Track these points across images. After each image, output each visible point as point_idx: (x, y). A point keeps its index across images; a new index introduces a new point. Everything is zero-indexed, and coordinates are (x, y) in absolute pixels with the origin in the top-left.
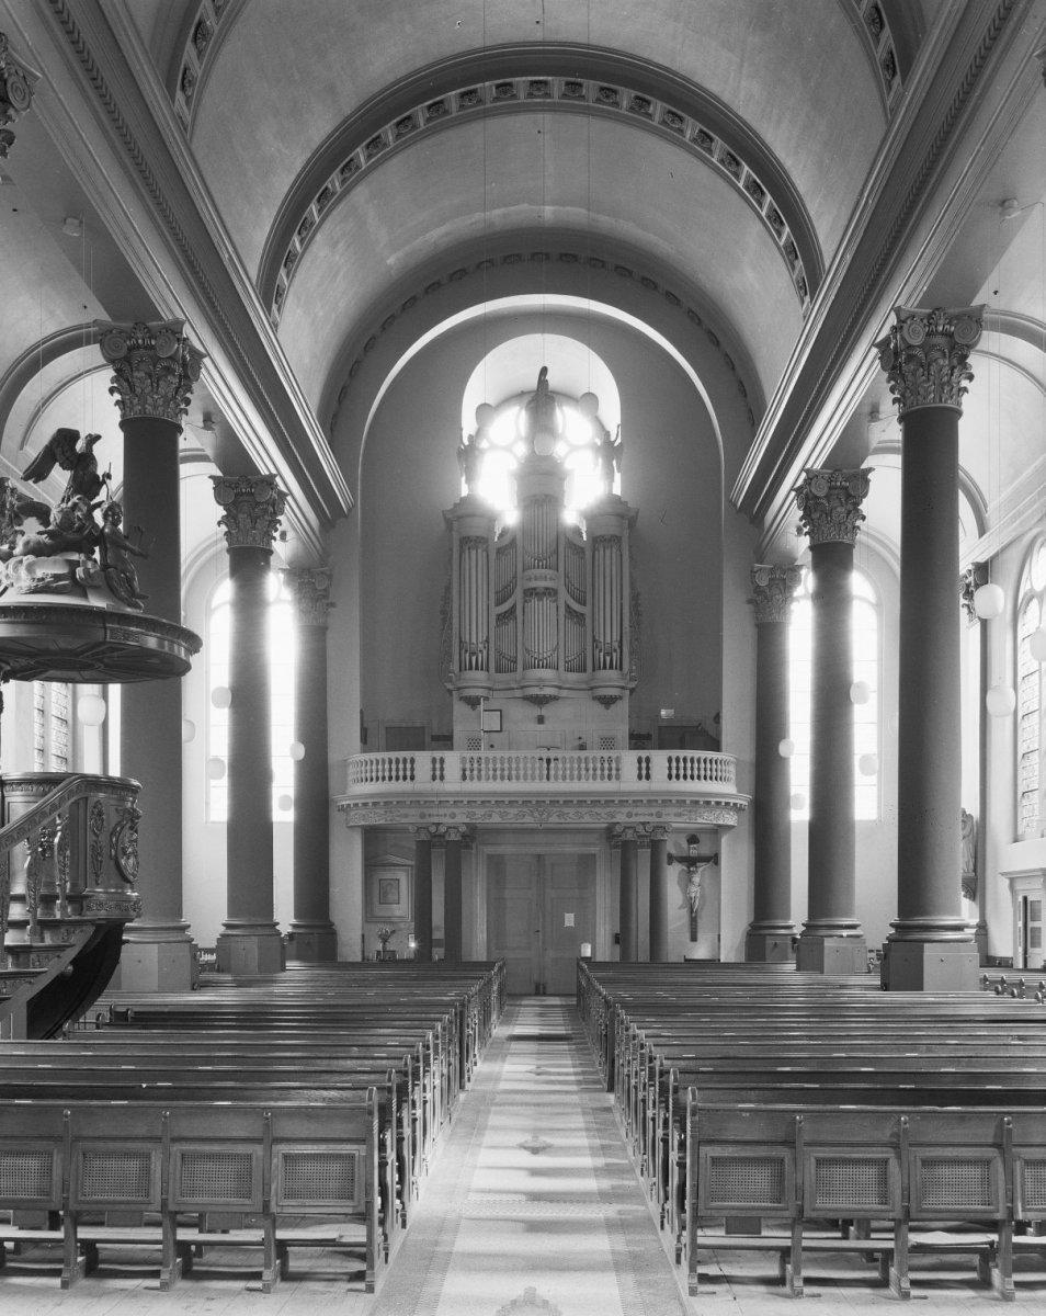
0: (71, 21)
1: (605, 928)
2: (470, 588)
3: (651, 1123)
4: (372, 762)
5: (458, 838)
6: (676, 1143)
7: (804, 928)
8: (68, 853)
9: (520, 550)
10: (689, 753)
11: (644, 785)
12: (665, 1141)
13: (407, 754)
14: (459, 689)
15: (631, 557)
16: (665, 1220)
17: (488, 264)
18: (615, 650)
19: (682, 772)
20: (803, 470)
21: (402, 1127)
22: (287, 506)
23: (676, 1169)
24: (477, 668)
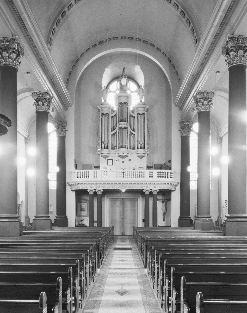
1: (140, 216)
2: (104, 131)
3: (159, 283)
4: (77, 173)
6: (157, 268)
7: (226, 218)
12: (154, 267)
13: (87, 171)
14: (101, 154)
15: (147, 119)
16: (154, 287)
17: (109, 40)
18: (143, 144)
19: (161, 176)
20: (192, 97)
21: (75, 286)
22: (53, 100)
23: (157, 274)
24: (106, 148)
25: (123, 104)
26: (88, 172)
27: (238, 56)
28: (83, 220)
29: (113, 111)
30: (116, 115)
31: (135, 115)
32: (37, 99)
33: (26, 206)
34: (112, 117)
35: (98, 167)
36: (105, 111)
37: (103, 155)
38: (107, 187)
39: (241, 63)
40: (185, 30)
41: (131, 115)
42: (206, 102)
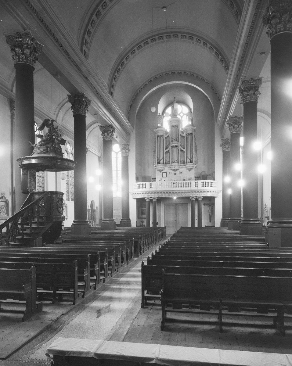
0: (53, 33)
5: (156, 200)
7: (73, 222)
8: (46, 207)
9: (170, 138)
10: (206, 181)
11: (196, 188)
13: (145, 183)
25: (175, 127)
26: (146, 184)
27: (250, 95)
28: (144, 221)
29: (166, 133)
30: (169, 136)
31: (185, 135)
32: (104, 131)
33: (100, 210)
34: (166, 138)
35: (155, 179)
36: (160, 134)
37: (159, 169)
38: (160, 196)
39: (252, 100)
40: (220, 66)
41: (181, 135)
42: (236, 126)
